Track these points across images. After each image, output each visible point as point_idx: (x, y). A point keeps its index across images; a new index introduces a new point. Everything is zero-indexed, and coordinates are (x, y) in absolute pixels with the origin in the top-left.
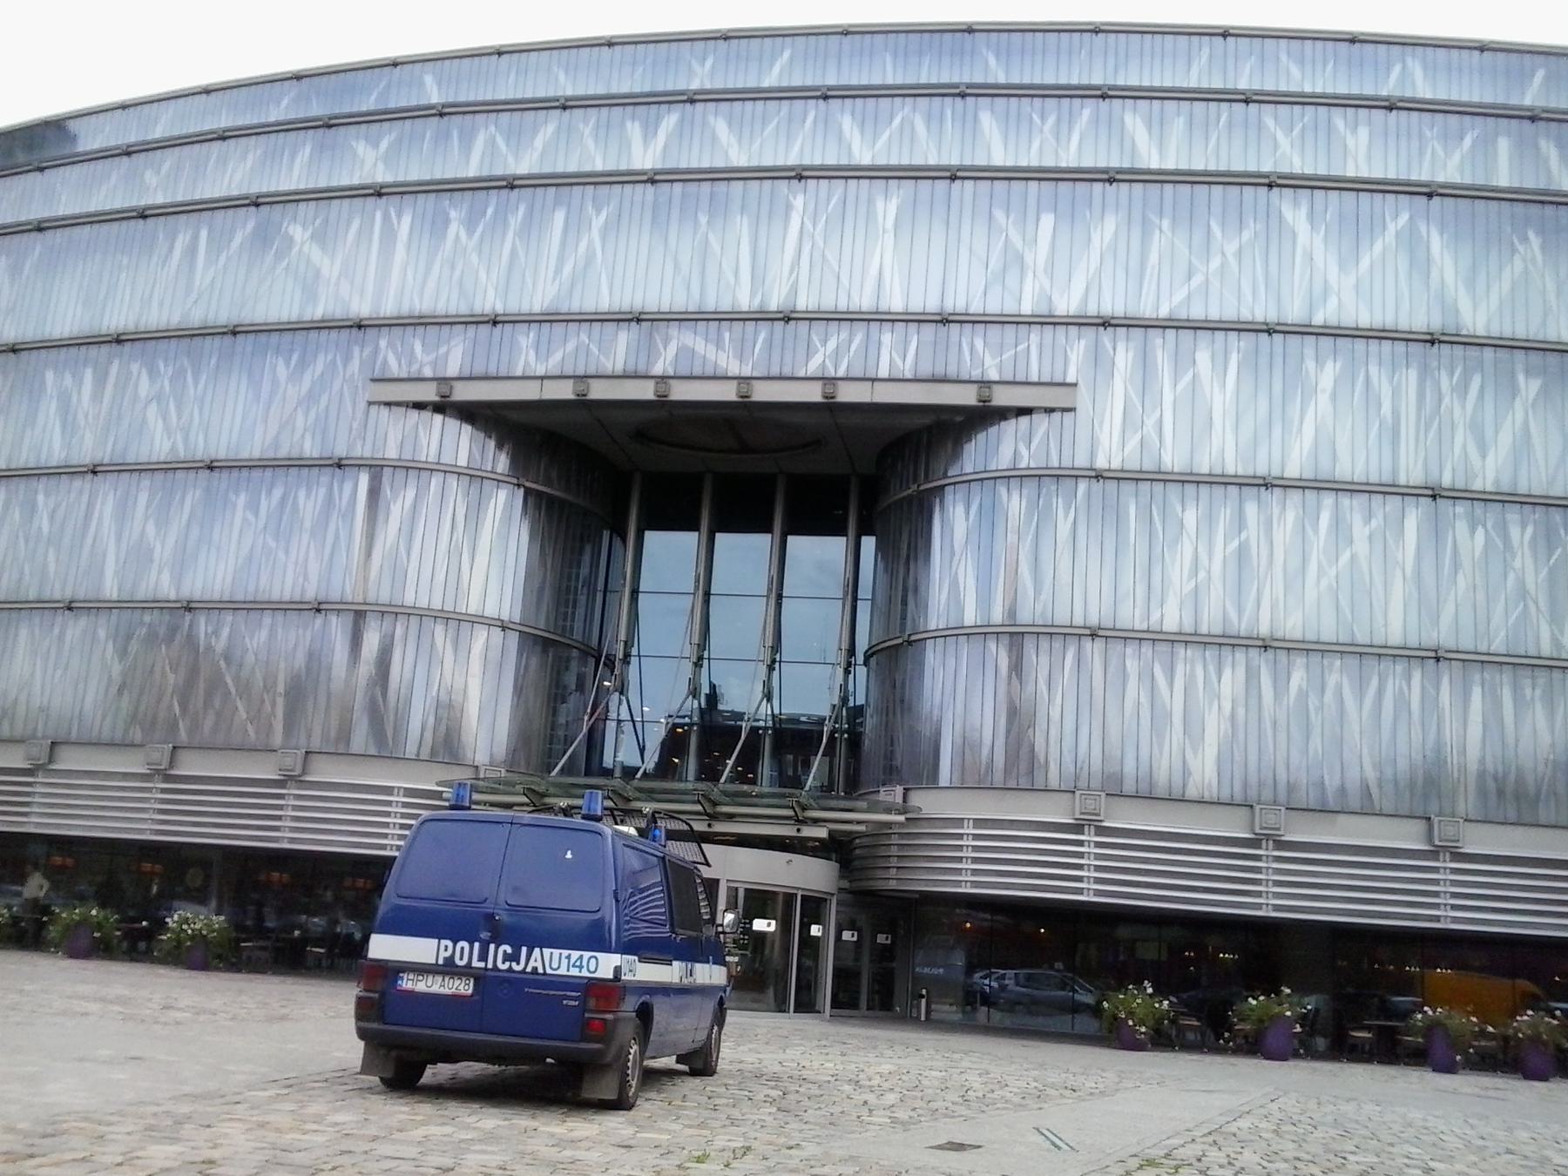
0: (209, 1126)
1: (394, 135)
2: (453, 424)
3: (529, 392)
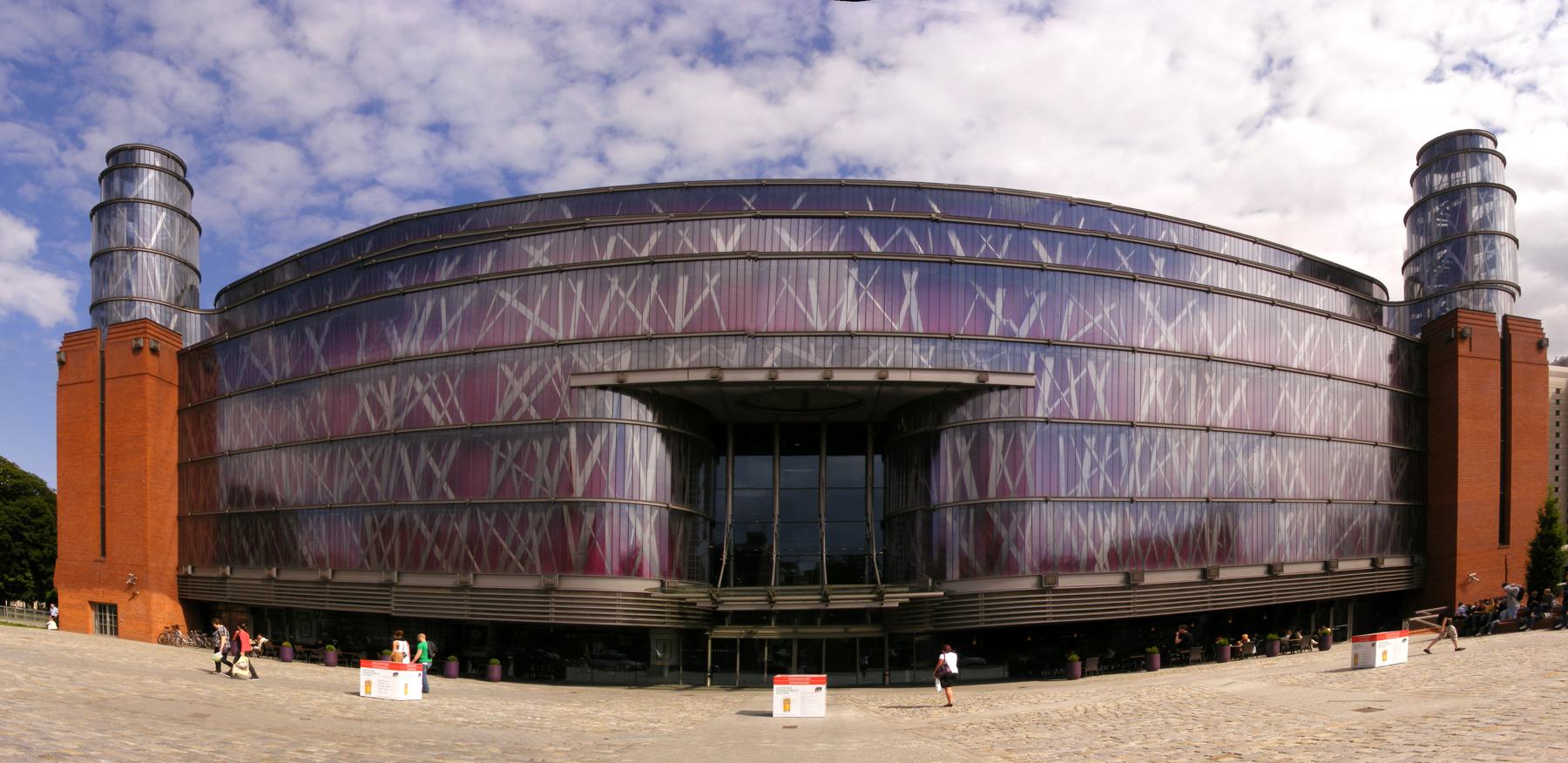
0: (1329, 701)
1: (744, 226)
3: (681, 377)
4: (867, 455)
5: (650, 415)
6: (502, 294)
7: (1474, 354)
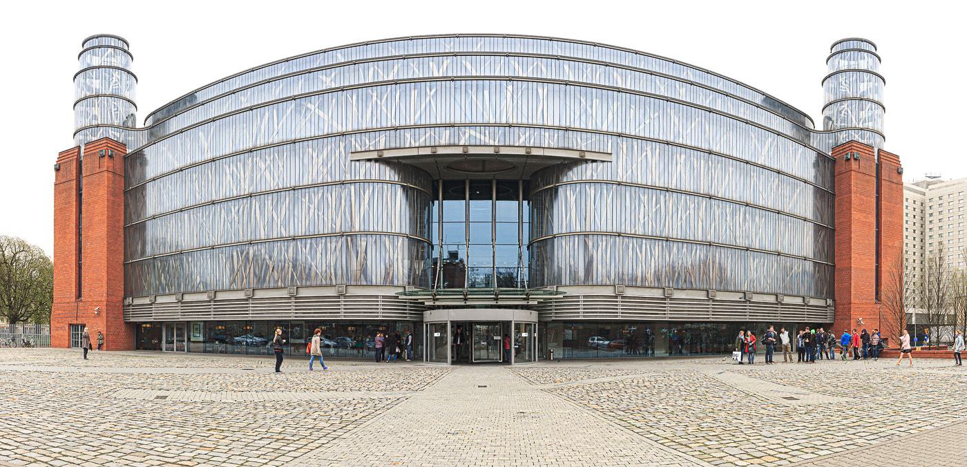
2: (383, 167)
3: (414, 153)
4: (519, 201)
5: (397, 177)
6: (309, 105)
7: (861, 171)
